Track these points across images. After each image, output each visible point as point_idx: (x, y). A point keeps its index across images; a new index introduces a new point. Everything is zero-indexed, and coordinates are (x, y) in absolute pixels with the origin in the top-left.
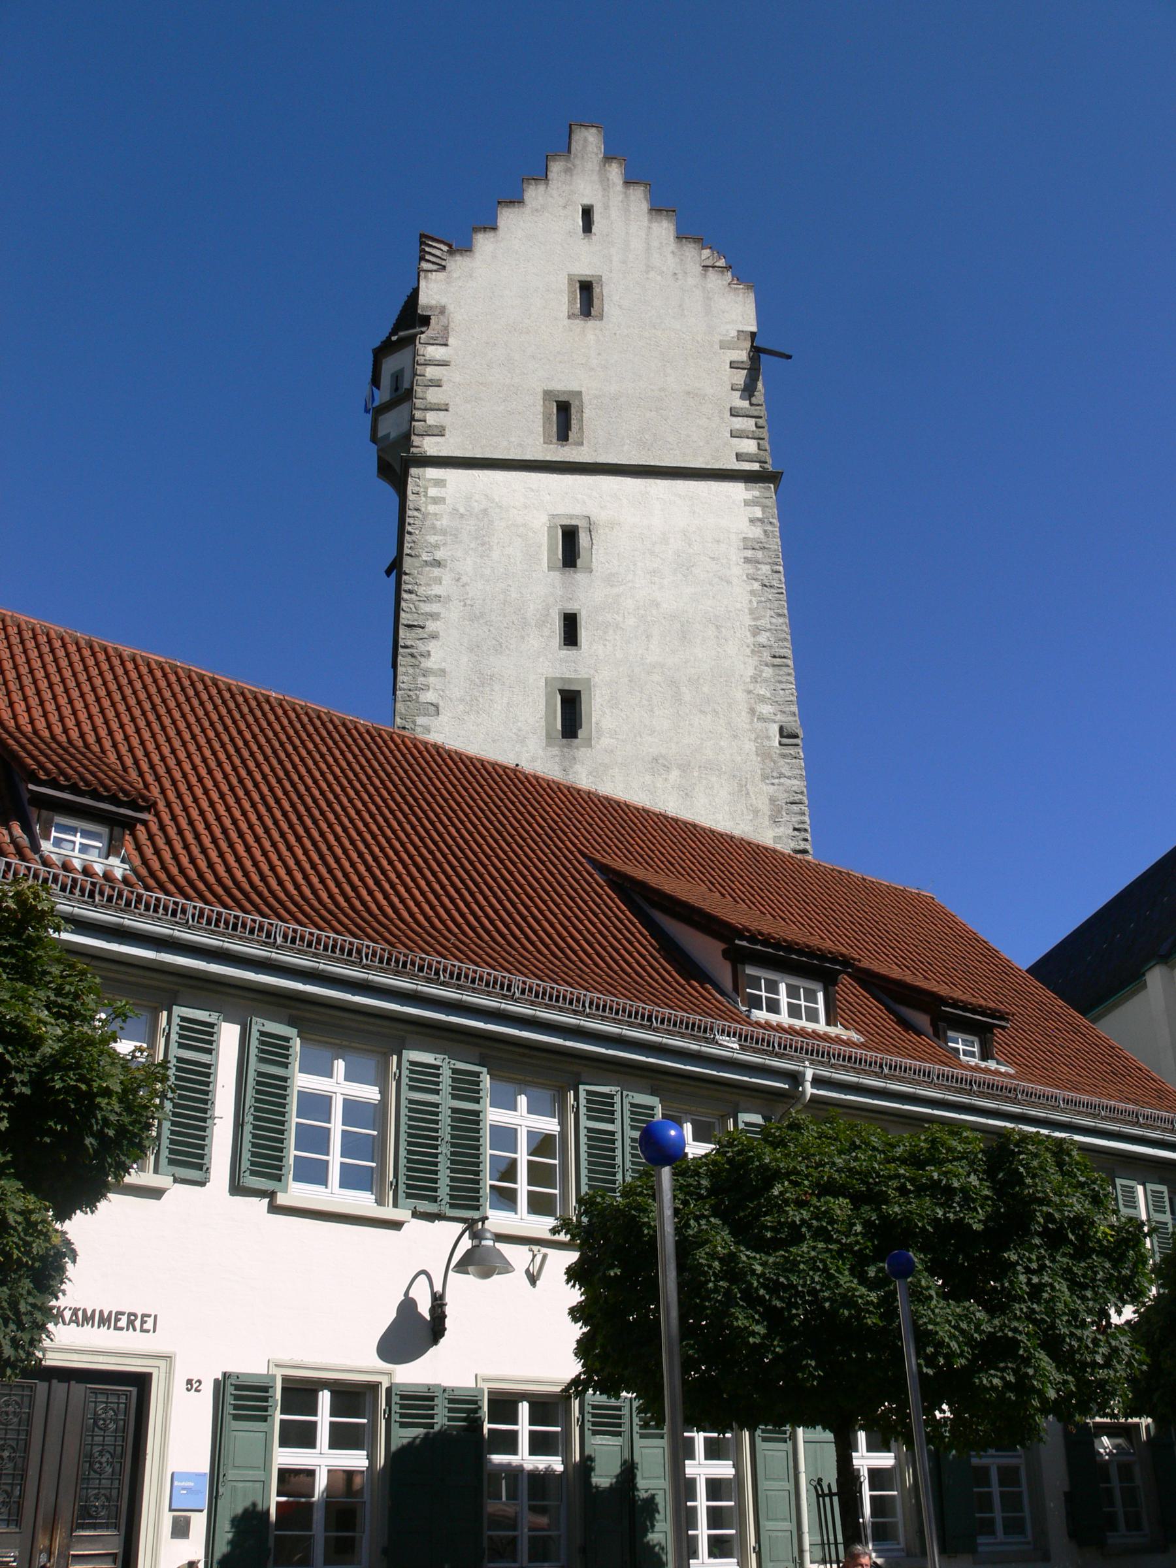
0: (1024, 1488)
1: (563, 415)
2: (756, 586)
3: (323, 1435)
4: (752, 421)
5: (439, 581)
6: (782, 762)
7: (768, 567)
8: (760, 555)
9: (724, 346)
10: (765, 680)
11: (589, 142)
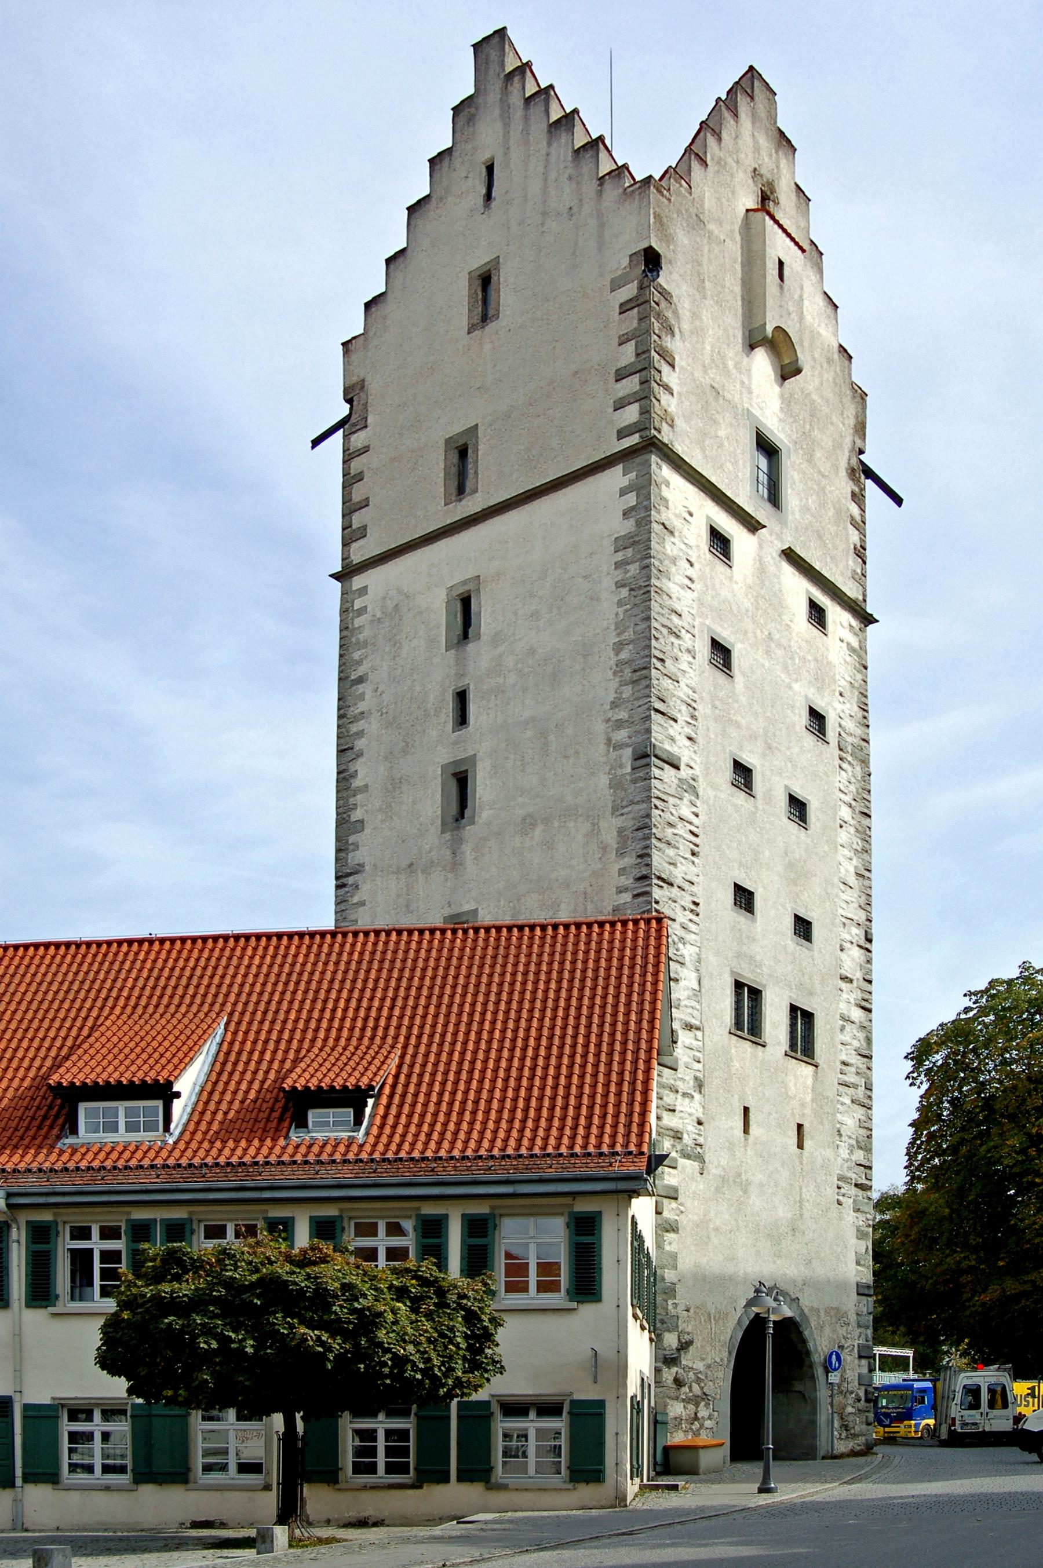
0: (411, 1444)
2: (624, 592)
3: (381, 1436)
4: (636, 378)
10: (626, 701)
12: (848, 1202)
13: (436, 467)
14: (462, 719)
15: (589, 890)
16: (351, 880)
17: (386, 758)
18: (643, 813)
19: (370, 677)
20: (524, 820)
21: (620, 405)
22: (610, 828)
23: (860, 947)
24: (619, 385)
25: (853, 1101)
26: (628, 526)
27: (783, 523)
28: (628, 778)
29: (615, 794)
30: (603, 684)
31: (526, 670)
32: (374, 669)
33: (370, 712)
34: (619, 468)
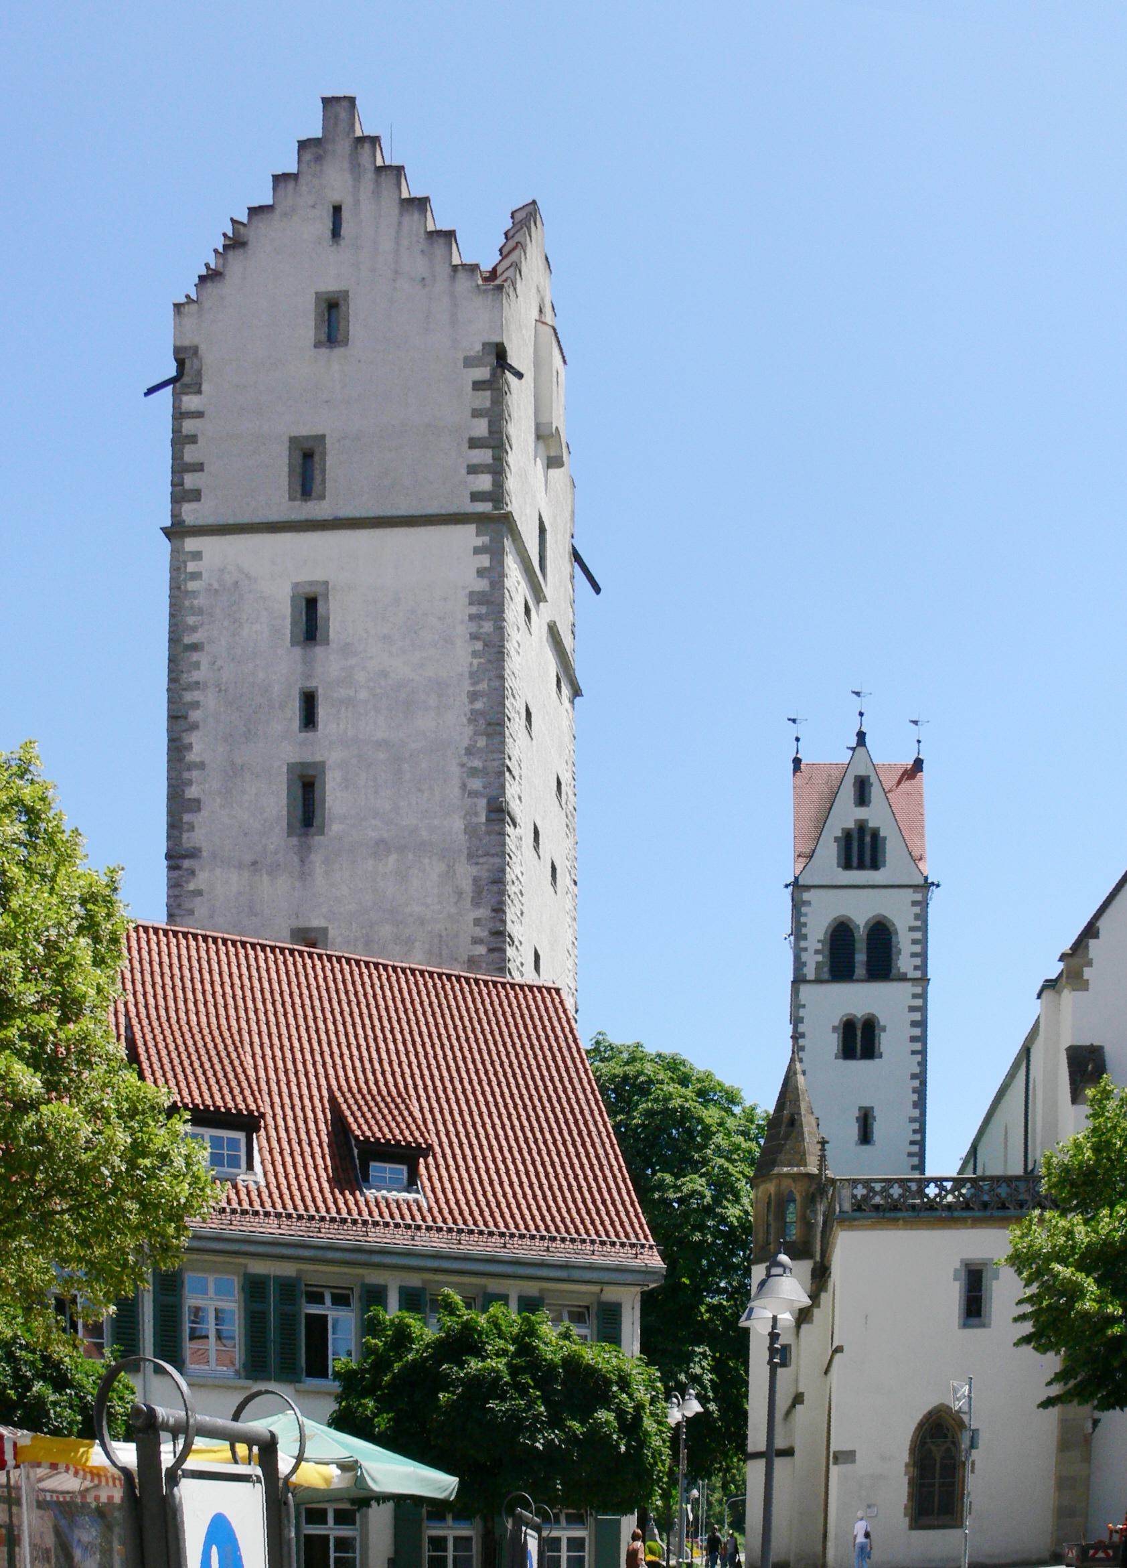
0: (358, 1555)
1: (307, 462)
2: (479, 646)
5: (197, 665)
8: (484, 609)
9: (469, 362)
10: (480, 750)
14: (309, 719)
15: (444, 933)
16: (186, 863)
19: (207, 647)
20: (377, 844)
21: (473, 470)
22: (465, 874)
28: (483, 828)
31: (378, 691)
33: (199, 592)
34: (471, 528)
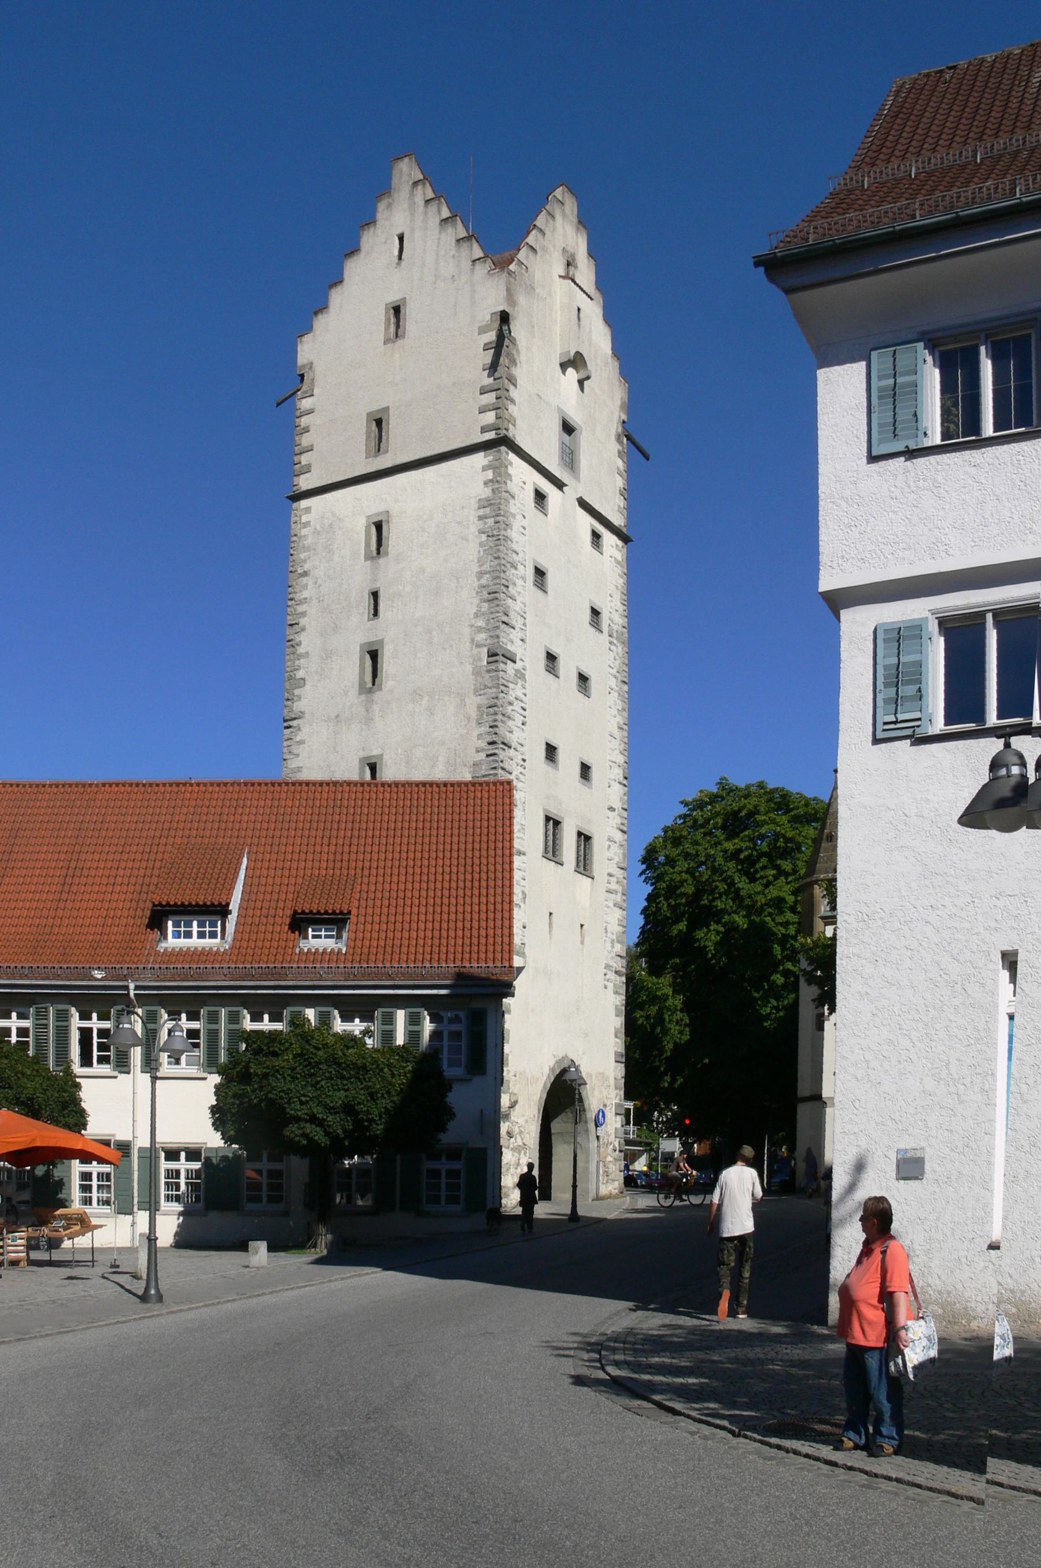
2: (484, 537)
4: (494, 394)
6: (487, 676)
7: (492, 520)
11: (406, 171)
12: (610, 986)
13: (360, 430)
16: (294, 723)
17: (321, 634)
18: (493, 695)
22: (473, 702)
23: (620, 783)
24: (483, 396)
25: (615, 905)
26: (487, 492)
27: (577, 478)
29: (476, 680)
30: (467, 600)
32: (314, 567)
34: (482, 454)
